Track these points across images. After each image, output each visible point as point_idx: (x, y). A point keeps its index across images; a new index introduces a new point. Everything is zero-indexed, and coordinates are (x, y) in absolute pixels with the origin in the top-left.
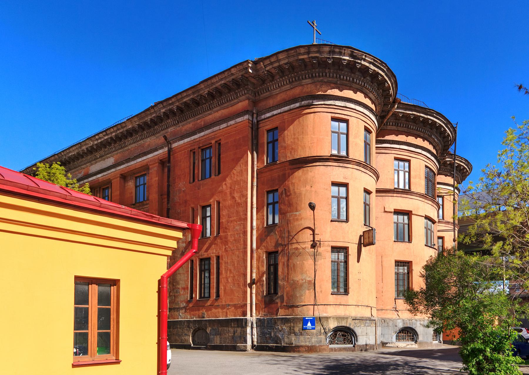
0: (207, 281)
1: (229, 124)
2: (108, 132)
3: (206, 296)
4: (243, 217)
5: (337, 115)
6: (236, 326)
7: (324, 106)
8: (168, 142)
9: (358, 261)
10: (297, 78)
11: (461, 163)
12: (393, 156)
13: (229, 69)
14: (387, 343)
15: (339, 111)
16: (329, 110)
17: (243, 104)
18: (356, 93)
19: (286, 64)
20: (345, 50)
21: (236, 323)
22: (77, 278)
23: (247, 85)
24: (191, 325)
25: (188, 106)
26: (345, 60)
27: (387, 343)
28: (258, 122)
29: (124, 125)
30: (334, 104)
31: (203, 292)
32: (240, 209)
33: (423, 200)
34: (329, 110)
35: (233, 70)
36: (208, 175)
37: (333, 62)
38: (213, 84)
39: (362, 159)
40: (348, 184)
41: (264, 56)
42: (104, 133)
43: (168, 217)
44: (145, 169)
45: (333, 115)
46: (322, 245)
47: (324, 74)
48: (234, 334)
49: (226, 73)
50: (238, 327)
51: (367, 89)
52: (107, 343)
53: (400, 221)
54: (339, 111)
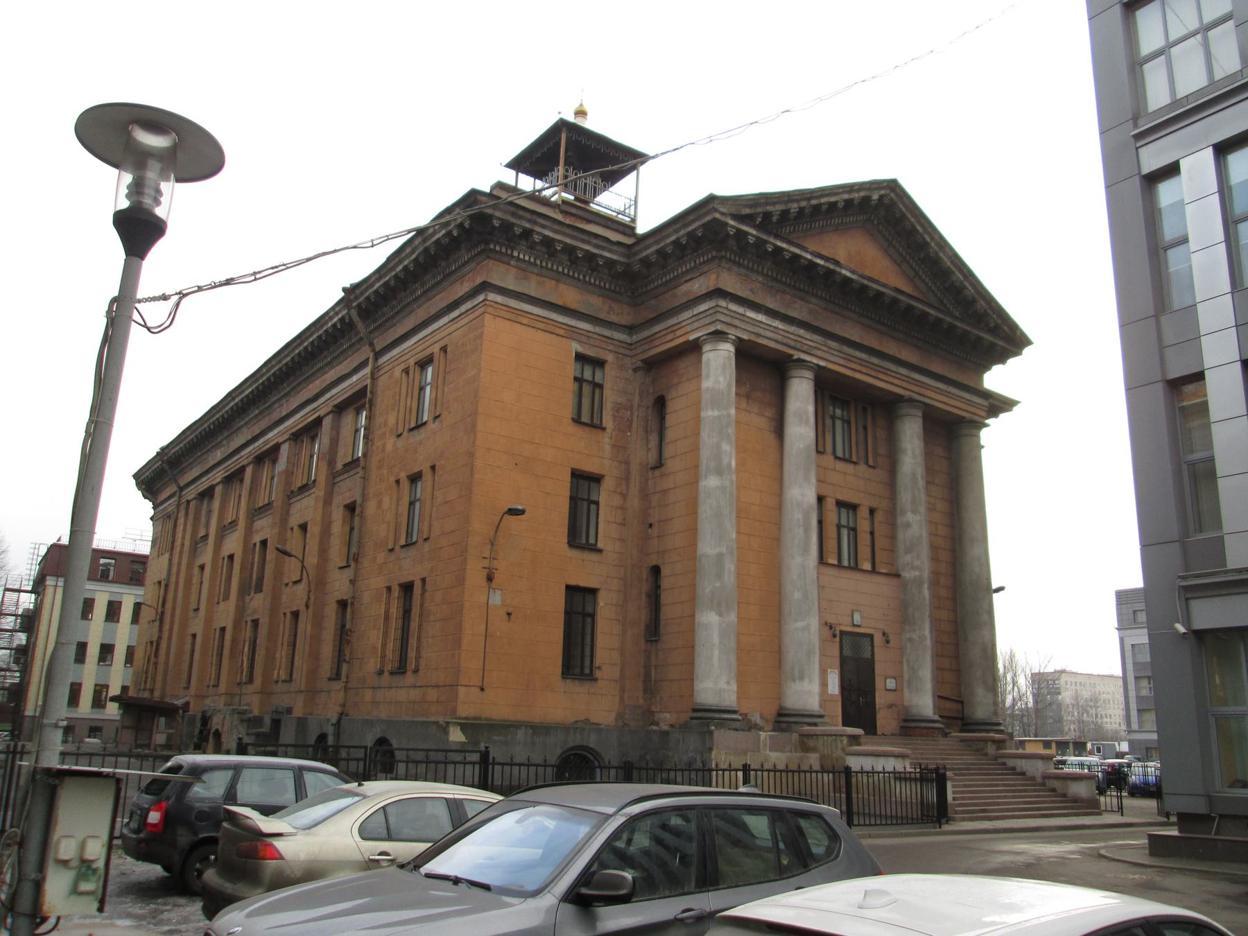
0: (525, 321)
3: (846, 563)
4: (497, 774)
9: (522, 512)
11: (690, 228)
18: (344, 290)
19: (499, 219)
22: (569, 589)
31: (174, 569)
32: (620, 844)
38: (535, 223)
39: (230, 773)
40: (136, 476)
43: (1139, 711)
52: (111, 603)
53: (404, 758)
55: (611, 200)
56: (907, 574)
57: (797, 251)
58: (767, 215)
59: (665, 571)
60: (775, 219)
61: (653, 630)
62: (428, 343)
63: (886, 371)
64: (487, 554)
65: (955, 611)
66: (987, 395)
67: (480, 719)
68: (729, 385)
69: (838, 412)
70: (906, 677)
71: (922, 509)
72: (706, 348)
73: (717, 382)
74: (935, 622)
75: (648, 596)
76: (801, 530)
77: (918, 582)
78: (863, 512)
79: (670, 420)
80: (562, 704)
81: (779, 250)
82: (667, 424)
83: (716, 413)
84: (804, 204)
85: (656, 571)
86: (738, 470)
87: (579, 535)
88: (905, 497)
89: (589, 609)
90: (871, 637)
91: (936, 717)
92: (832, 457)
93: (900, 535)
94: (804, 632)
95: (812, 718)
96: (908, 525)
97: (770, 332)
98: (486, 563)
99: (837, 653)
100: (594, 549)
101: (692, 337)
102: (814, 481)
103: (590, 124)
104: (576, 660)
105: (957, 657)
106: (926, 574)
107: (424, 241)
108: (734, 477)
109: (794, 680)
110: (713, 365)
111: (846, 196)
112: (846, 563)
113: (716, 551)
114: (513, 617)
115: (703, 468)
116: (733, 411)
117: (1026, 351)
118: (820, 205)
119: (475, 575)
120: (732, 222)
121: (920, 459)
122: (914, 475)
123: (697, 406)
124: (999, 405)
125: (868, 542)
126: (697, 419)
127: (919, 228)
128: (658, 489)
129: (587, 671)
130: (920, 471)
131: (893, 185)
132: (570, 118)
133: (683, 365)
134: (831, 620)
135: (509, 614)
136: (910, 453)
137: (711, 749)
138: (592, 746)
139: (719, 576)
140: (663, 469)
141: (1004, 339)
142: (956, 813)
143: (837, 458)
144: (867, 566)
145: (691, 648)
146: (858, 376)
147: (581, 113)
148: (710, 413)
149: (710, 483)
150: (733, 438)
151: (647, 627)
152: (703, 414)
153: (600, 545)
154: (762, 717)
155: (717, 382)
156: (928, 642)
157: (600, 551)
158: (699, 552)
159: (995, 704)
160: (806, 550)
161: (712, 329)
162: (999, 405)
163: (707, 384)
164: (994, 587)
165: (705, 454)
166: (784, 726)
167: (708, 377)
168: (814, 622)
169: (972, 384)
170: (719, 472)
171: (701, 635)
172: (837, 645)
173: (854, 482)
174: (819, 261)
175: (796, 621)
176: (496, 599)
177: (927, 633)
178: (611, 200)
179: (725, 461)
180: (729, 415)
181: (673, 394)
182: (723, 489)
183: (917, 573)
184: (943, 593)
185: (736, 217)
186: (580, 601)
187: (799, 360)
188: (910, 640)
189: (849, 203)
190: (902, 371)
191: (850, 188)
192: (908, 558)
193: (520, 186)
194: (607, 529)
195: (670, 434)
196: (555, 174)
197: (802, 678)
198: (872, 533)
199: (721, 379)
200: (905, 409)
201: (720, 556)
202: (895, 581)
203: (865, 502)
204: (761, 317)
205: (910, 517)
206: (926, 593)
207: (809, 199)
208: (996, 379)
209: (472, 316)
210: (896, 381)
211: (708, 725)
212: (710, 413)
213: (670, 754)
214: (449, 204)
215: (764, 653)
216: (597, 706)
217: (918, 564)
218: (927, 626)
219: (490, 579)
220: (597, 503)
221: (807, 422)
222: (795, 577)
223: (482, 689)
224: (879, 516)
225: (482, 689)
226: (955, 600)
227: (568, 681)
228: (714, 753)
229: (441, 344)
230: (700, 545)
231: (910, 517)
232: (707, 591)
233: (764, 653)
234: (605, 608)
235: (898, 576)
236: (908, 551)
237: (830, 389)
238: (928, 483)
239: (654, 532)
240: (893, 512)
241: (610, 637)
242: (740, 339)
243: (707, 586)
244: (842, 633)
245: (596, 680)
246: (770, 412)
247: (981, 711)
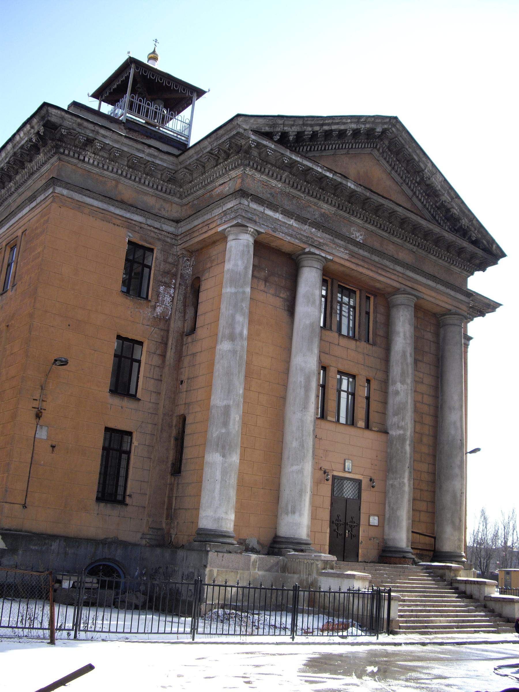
1: (224, 209)
3: (343, 420)
55: (175, 125)
56: (393, 433)
57: (310, 164)
58: (284, 135)
59: (189, 420)
60: (291, 138)
61: (177, 469)
62: (15, 229)
63: (384, 268)
64: (37, 397)
65: (434, 465)
66: (470, 294)
67: (21, 531)
68: (246, 268)
69: (346, 299)
70: (387, 516)
71: (409, 381)
72: (230, 238)
73: (236, 265)
74: (414, 471)
75: (176, 439)
76: (302, 391)
77: (402, 439)
78: (361, 381)
79: (202, 296)
80: (93, 521)
81: (294, 163)
82: (200, 301)
83: (233, 290)
84: (317, 128)
85: (183, 419)
86: (250, 338)
87: (122, 385)
88: (396, 370)
89: (125, 447)
90: (359, 482)
91: (409, 549)
92: (336, 335)
93: (391, 401)
94: (301, 476)
95: (299, 545)
96: (397, 393)
97: (287, 230)
98: (36, 404)
99: (329, 494)
100: (134, 397)
101: (220, 229)
102: (316, 351)
103: (158, 66)
104: (111, 490)
105: (433, 502)
106: (409, 433)
107: (14, 147)
108: (245, 343)
109: (287, 514)
110: (234, 251)
111: (354, 126)
112: (343, 420)
113: (225, 403)
114: (55, 449)
115: (220, 334)
116: (248, 290)
117: (501, 261)
118: (332, 131)
119: (27, 415)
120: (253, 137)
121: (410, 341)
122: (404, 353)
123: (220, 285)
124: (484, 306)
125: (365, 405)
126: (220, 295)
127: (415, 157)
128: (189, 353)
129: (120, 498)
130: (409, 350)
131: (394, 121)
132: (144, 60)
133: (214, 251)
134: (326, 466)
135: (53, 447)
136: (402, 335)
137: (205, 566)
138: (117, 559)
139: (225, 424)
140: (194, 336)
141: (487, 253)
142: (400, 627)
143: (340, 334)
144: (361, 424)
145: (200, 482)
146: (361, 269)
147: (153, 57)
148: (228, 290)
149: (224, 346)
150: (247, 311)
151: (173, 464)
152: (224, 291)
153: (139, 395)
154: (259, 543)
155: (236, 265)
156: (407, 488)
157: (139, 400)
158: (211, 404)
159: (460, 540)
160: (305, 407)
161: (235, 222)
162: (484, 306)
163: (228, 266)
164: (470, 449)
165: (222, 323)
166: (276, 550)
167: (229, 260)
168: (308, 467)
169: (457, 284)
170: (232, 338)
171: (207, 472)
172: (329, 488)
173: (352, 355)
174: (330, 175)
175: (292, 465)
176: (42, 434)
177: (406, 480)
178: (175, 125)
179: (238, 330)
180: (244, 293)
181: (206, 275)
182: (234, 352)
183: (401, 432)
184: (425, 450)
185: (256, 132)
186: (116, 444)
187: (310, 253)
188: (392, 485)
189: (356, 133)
190: (399, 268)
191: (357, 119)
192: (395, 419)
193: (102, 110)
194: (144, 380)
195: (201, 309)
196: (124, 100)
197: (293, 512)
198: (368, 398)
199: (240, 263)
200: (400, 298)
201: (227, 408)
202: (383, 436)
203: (363, 373)
204: (278, 216)
205: (399, 386)
206: (408, 448)
207: (322, 125)
208: (478, 282)
209: (44, 206)
210: (393, 277)
211: (205, 545)
212: (228, 290)
213: (177, 569)
214: (29, 117)
215: (266, 489)
216: (124, 525)
217: (404, 425)
218: (407, 474)
219: (38, 416)
220: (139, 362)
221: (314, 302)
222: (294, 429)
223: (25, 506)
224: (374, 385)
225: (25, 506)
226: (434, 456)
227: (102, 505)
228: (208, 570)
229: (23, 228)
230: (212, 398)
231: (399, 386)
232: (215, 435)
233: (266, 489)
234: (137, 446)
235: (386, 433)
236: (396, 414)
237: (334, 280)
238: (416, 361)
239: (184, 387)
240: (385, 383)
241: (141, 472)
242: (259, 233)
243: (215, 432)
244: (334, 477)
245: (127, 505)
246: (284, 294)
247: (447, 547)
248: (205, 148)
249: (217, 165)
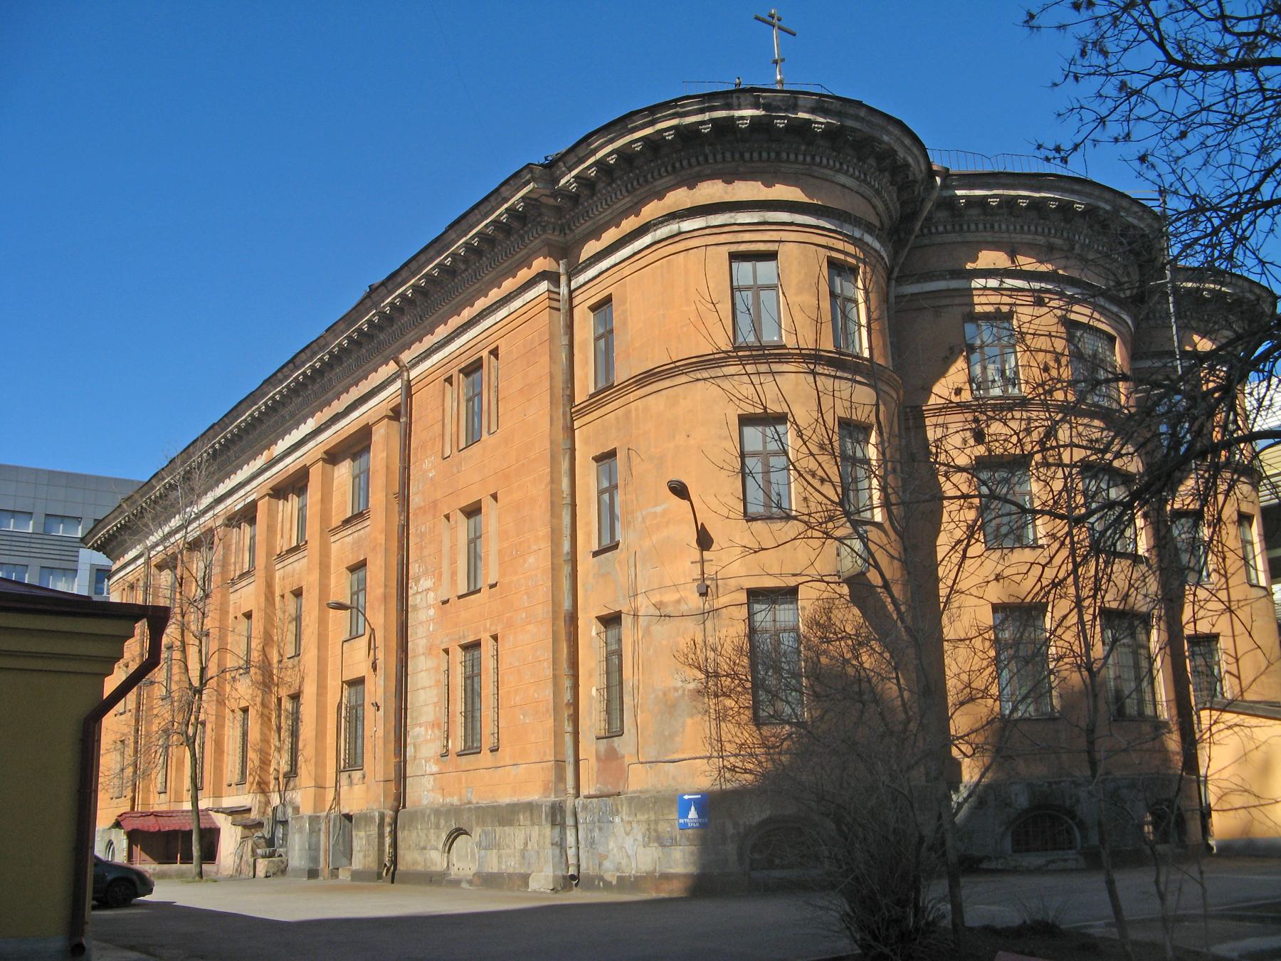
2: (298, 361)
5: (743, 248)
6: (528, 823)
7: (707, 231)
8: (403, 369)
10: (641, 180)
12: (725, 250)
13: (497, 190)
14: (981, 860)
15: (747, 236)
16: (723, 239)
17: (863, 345)
20: (738, 98)
21: (528, 814)
23: (540, 215)
24: (442, 822)
25: (913, 458)
26: (742, 118)
27: (981, 860)
28: (571, 292)
29: (322, 342)
30: (733, 221)
33: (295, 558)
34: (723, 239)
35: (503, 189)
36: (488, 741)
37: (787, 125)
39: (622, 373)
41: (570, 146)
42: (291, 366)
44: (364, 435)
45: (734, 248)
46: (721, 590)
47: (701, 159)
48: (526, 844)
49: (492, 199)
50: (533, 824)
51: (825, 167)
54: (747, 236)
248: (889, 133)
249: (525, 225)
